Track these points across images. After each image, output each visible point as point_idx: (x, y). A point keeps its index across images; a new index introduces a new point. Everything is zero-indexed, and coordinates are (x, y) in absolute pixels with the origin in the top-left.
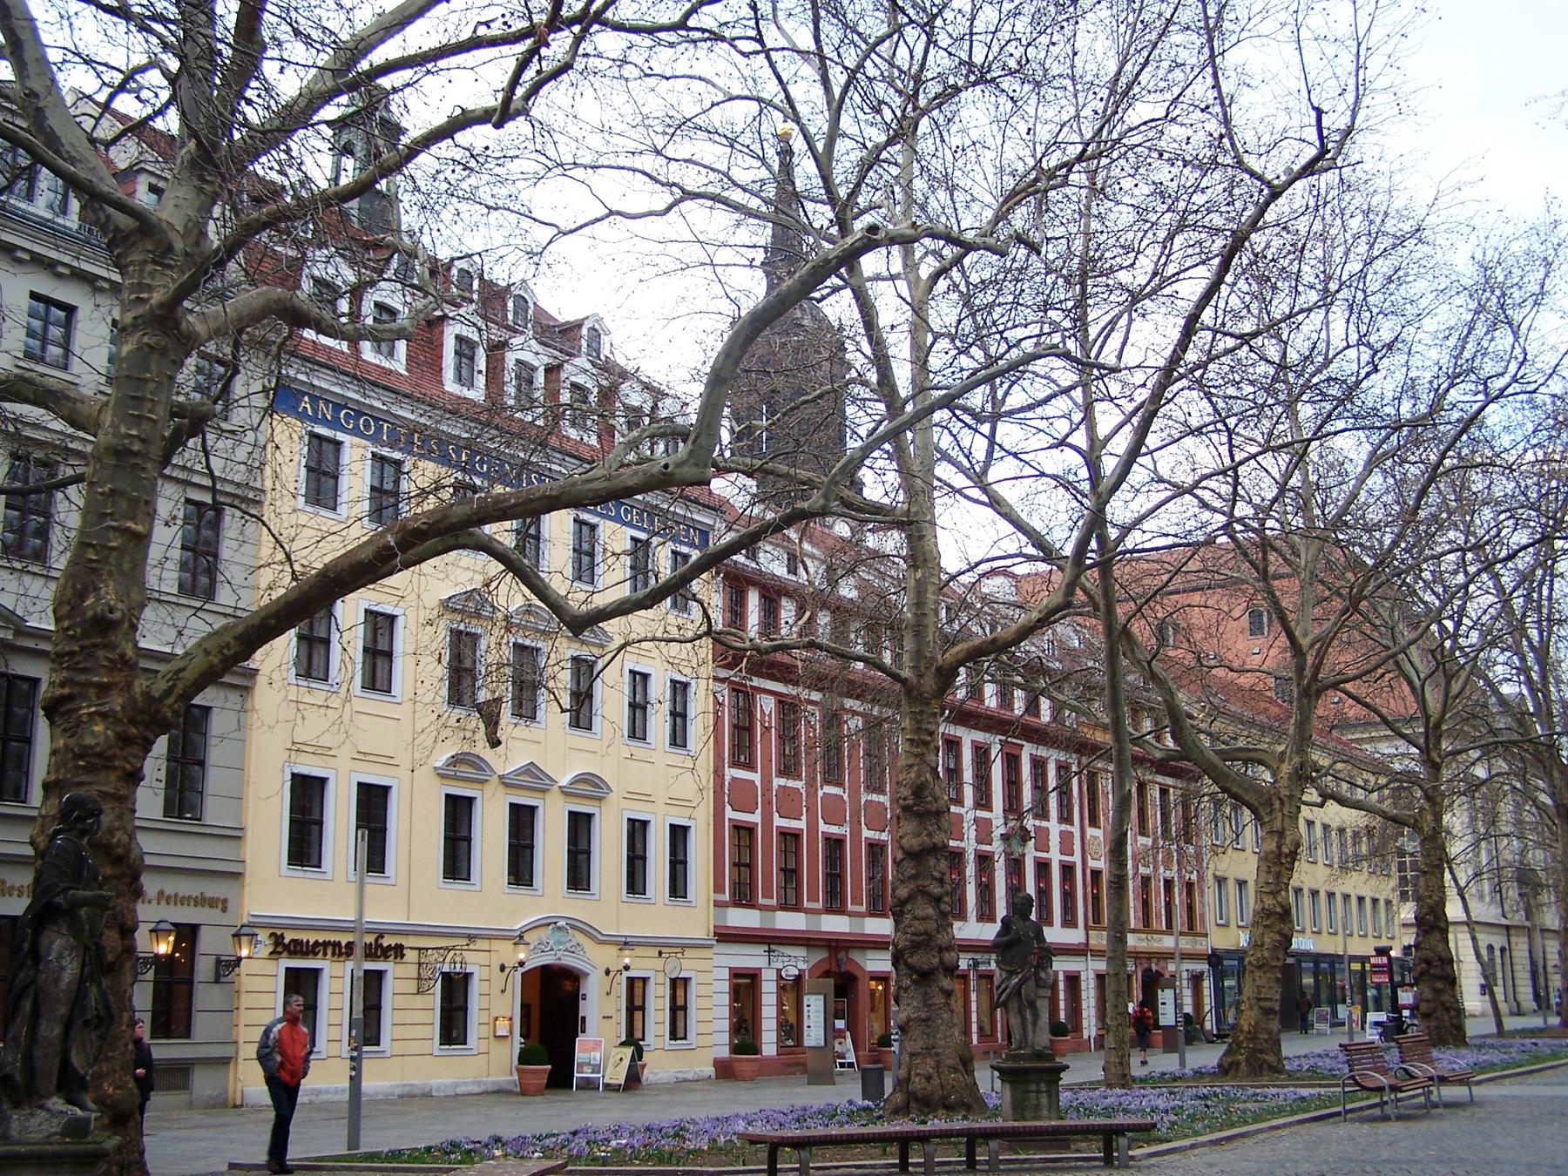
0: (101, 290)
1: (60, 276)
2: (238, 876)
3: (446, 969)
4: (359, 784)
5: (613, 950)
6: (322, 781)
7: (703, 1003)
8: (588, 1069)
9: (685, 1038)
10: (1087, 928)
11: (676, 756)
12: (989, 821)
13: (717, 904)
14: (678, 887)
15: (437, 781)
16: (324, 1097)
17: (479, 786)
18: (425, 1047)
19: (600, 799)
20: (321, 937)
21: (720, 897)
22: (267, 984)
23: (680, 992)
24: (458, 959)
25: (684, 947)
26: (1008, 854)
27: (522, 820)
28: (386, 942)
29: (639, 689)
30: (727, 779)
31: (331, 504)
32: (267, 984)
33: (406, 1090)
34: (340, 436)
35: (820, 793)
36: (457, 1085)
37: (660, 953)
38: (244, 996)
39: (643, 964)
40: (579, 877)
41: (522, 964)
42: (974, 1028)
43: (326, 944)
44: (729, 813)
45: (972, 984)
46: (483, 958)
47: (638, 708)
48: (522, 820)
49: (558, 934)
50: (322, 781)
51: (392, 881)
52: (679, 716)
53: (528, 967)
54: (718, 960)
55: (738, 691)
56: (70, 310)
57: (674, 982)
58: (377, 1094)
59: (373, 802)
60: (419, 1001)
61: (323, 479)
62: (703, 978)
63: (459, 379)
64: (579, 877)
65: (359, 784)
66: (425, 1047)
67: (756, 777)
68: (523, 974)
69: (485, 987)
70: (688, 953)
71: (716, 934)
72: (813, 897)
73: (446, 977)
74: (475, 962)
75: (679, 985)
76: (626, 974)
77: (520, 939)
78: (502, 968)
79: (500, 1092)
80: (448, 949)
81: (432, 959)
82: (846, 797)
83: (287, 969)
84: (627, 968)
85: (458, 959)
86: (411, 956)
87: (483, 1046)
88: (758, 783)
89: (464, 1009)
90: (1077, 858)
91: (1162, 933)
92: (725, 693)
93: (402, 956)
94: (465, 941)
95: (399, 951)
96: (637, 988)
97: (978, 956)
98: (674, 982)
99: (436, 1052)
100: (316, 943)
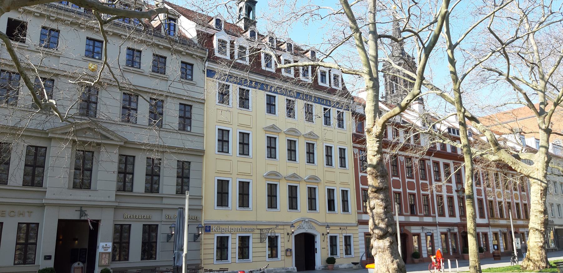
0: (82, 28)
1: (161, 48)
2: (201, 210)
3: (269, 235)
4: (239, 182)
7: (263, 250)
9: (351, 254)
10: (488, 218)
12: (451, 187)
13: (358, 213)
14: (345, 209)
15: (265, 180)
19: (318, 183)
23: (348, 240)
24: (273, 232)
25: (277, 225)
26: (458, 197)
27: (293, 191)
29: (329, 151)
31: (247, 107)
35: (391, 179)
37: (340, 228)
39: (333, 232)
40: (312, 206)
41: (293, 233)
42: (451, 250)
45: (449, 237)
46: (282, 231)
47: (329, 156)
48: (293, 191)
51: (300, 211)
52: (342, 158)
53: (296, 233)
54: (360, 230)
55: (435, 163)
56: (192, 65)
59: (244, 187)
60: (260, 245)
61: (271, 106)
62: (355, 236)
64: (312, 206)
65: (239, 182)
67: (414, 181)
68: (295, 236)
70: (348, 228)
72: (421, 212)
73: (269, 237)
74: (278, 232)
75: (347, 239)
77: (292, 226)
78: (288, 234)
80: (270, 229)
82: (400, 180)
83: (218, 237)
85: (273, 232)
88: (415, 182)
89: (336, 245)
90: (483, 197)
91: (499, 219)
94: (275, 226)
96: (333, 240)
97: (450, 228)
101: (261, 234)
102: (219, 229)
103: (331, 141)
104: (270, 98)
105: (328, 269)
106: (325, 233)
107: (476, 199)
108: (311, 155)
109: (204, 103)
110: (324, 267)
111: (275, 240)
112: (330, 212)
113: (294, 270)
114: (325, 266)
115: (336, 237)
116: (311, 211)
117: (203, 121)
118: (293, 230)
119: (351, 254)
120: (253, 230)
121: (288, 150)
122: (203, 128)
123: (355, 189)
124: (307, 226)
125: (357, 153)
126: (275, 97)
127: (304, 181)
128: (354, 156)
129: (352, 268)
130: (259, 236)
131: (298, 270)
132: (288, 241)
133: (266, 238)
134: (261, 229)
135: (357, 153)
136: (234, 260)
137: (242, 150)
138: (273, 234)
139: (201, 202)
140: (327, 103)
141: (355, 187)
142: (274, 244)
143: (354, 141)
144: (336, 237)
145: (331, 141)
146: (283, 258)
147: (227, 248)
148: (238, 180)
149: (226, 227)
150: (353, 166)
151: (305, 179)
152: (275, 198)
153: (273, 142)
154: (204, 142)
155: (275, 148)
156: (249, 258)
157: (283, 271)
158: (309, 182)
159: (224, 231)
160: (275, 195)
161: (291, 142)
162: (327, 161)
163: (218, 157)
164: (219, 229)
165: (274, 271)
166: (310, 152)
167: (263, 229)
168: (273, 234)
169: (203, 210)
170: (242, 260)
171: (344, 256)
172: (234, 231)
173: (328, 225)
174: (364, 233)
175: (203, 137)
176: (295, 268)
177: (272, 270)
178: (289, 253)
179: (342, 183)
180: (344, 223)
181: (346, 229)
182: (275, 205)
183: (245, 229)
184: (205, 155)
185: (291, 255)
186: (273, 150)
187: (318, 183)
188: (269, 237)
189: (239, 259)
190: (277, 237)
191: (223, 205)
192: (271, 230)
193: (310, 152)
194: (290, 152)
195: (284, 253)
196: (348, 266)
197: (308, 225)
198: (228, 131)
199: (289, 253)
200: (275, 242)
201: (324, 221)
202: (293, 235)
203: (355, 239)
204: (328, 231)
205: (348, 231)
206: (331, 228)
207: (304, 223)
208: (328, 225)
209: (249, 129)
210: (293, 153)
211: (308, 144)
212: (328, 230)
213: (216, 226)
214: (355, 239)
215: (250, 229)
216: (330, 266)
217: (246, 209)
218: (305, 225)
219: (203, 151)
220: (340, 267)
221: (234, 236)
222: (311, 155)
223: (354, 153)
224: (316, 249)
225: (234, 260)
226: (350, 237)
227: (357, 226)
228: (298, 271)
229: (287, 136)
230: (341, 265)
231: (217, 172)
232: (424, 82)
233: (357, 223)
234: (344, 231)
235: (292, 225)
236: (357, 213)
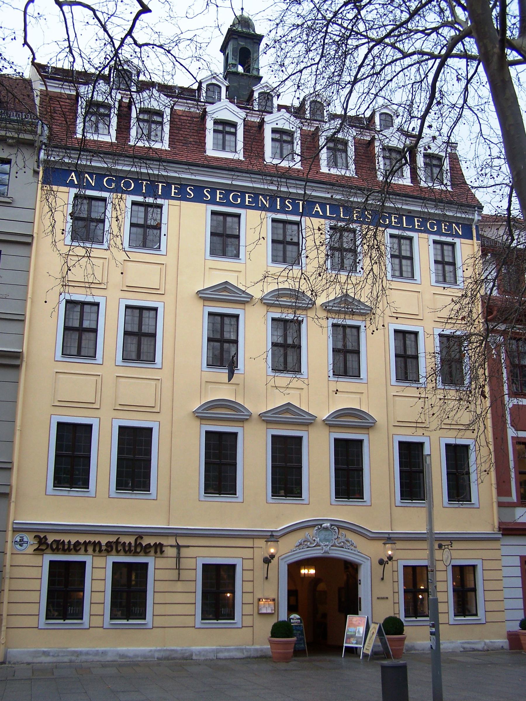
5: (380, 544)
6: (150, 430)
8: (353, 641)
9: (476, 615)
13: (501, 505)
15: (198, 422)
16: (83, 658)
17: (365, 431)
18: (189, 621)
20: (82, 539)
22: (34, 573)
28: (145, 542)
32: (34, 573)
33: (167, 654)
34: (159, 201)
36: (218, 651)
38: (7, 581)
43: (86, 544)
44: (511, 432)
46: (247, 553)
49: (324, 534)
50: (150, 430)
54: (505, 550)
58: (137, 656)
62: (488, 565)
66: (189, 621)
69: (248, 576)
70: (455, 545)
71: (500, 529)
79: (262, 658)
86: (171, 552)
87: (248, 621)
93: (162, 552)
95: (159, 548)
100: (78, 543)
104: (225, 221)
107: (421, 441)
109: (30, 244)
119: (476, 615)
126: (238, 216)
136: (97, 621)
139: (10, 477)
148: (117, 424)
161: (285, 330)
163: (122, 372)
174: (521, 557)
175: (23, 321)
198: (416, 334)
203: (488, 575)
214: (488, 575)
219: (18, 356)
224: (360, 598)
225: (97, 621)
229: (207, 303)
232: (68, 50)
236: (495, 505)
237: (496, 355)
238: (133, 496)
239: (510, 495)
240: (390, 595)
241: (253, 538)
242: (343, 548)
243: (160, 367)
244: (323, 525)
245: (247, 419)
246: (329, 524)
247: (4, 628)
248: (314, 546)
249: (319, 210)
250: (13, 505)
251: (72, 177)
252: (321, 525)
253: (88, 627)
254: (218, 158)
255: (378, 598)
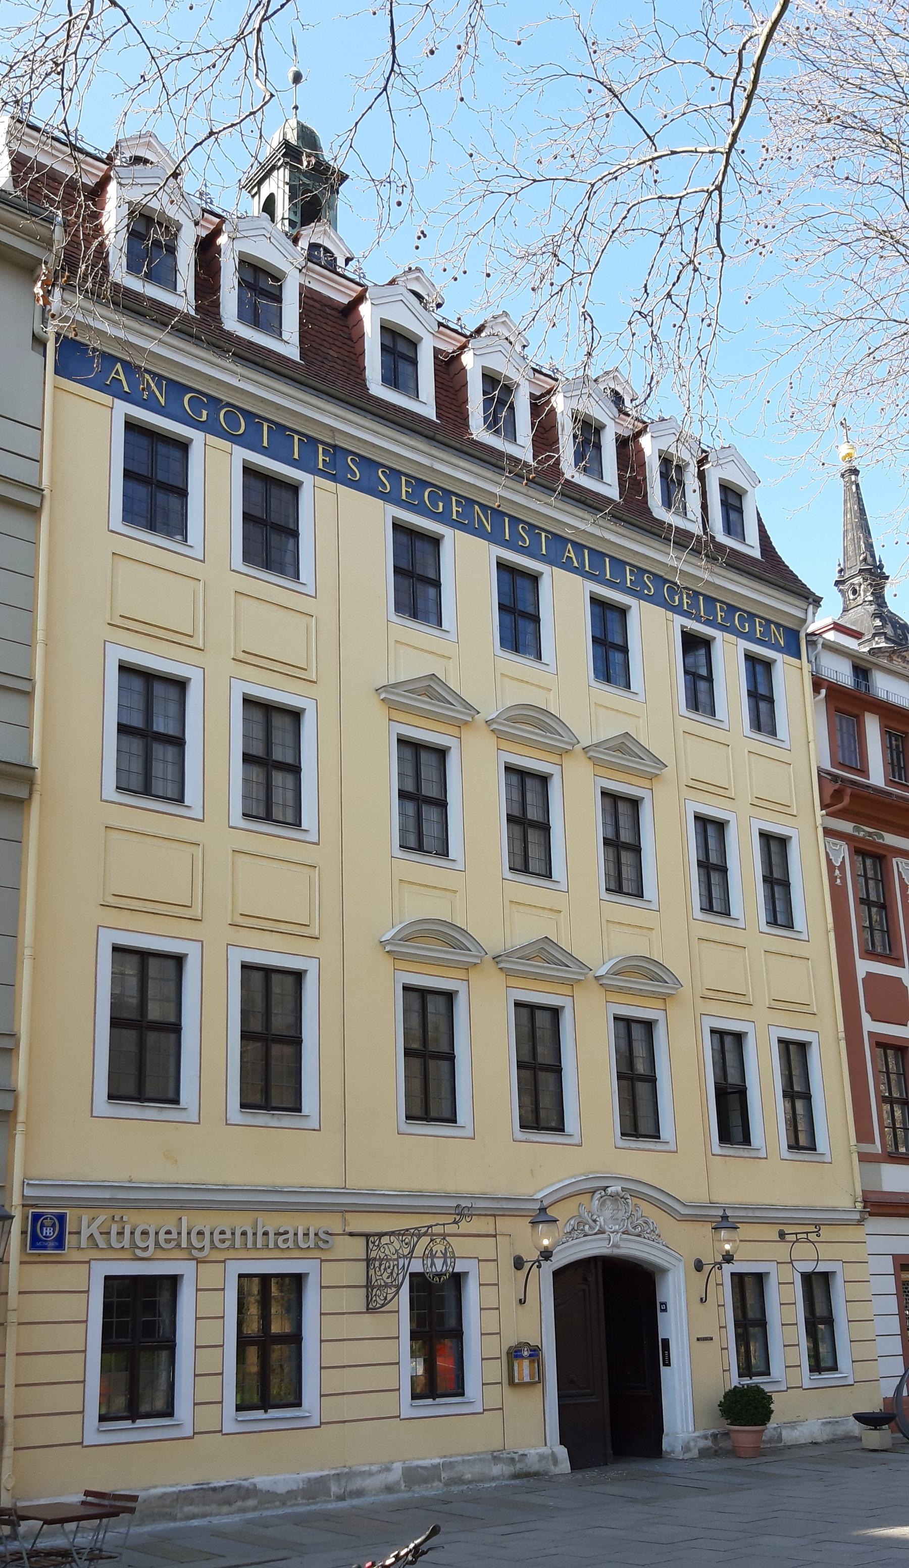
3: (417, 1266)
9: (834, 1368)
11: (777, 939)
13: (864, 1158)
15: (386, 964)
19: (664, 998)
21: (867, 1148)
23: (818, 1293)
24: (439, 1248)
25: (461, 1213)
30: (861, 975)
37: (782, 1235)
38: (12, 1332)
41: (547, 1254)
44: (869, 1025)
46: (485, 1248)
51: (576, 1140)
53: (560, 1260)
54: (876, 1244)
57: (807, 1278)
60: (368, 1324)
62: (853, 1272)
63: (492, 424)
68: (557, 1274)
70: (826, 1233)
73: (419, 1282)
76: (728, 1269)
78: (519, 1263)
81: (389, 1251)
83: (107, 1278)
84: (728, 1258)
85: (439, 1248)
89: (762, 1323)
92: (841, 853)
98: (807, 1278)
99: (406, 1412)
101: (369, 1261)
102: (120, 1233)
103: (721, 792)
105: (733, 1453)
106: (707, 1259)
108: (627, 857)
109: (34, 512)
110: (709, 1443)
111: (450, 1294)
112: (729, 1150)
113: (555, 1462)
114: (714, 1436)
115: (760, 1278)
116: (632, 1143)
117: (31, 611)
118: (546, 1242)
119: (834, 1368)
120: (323, 1240)
121: (511, 819)
122: (30, 646)
123: (842, 1035)
124: (614, 1219)
125: (843, 862)
127: (594, 983)
128: (832, 879)
129: (859, 1439)
130: (357, 1273)
131: (576, 1463)
132: (522, 1302)
133: (399, 1287)
134: (367, 1236)
135: (843, 862)
136: (208, 1418)
137: (262, 796)
138: (439, 1263)
140: (694, 604)
141: (841, 1027)
142: (441, 1317)
143: (828, 800)
144: (760, 1278)
145: (721, 792)
146: (494, 1396)
147: (170, 1346)
148: (237, 957)
149: (167, 1220)
150: (831, 925)
151: (602, 971)
152: (444, 1065)
153: (428, 772)
154: (28, 727)
155: (442, 804)
156: (299, 1405)
157: (497, 1470)
158: (620, 990)
159: (151, 1242)
160: (444, 1048)
162: (704, 892)
164: (120, 1233)
165: (444, 1475)
166: (623, 839)
167: (381, 1235)
168: (439, 1263)
169: (21, 1117)
170: (259, 1414)
171: (806, 1377)
172: (213, 1247)
173: (725, 1218)
174: (895, 1256)
175: (28, 694)
176: (562, 1452)
177: (436, 1467)
178: (524, 1369)
179: (779, 1005)
180: (797, 1209)
181: (812, 1237)
182: (446, 1103)
183: (278, 1234)
184: (36, 798)
185: (539, 1379)
186: (430, 814)
187: (664, 998)
188: (419, 1282)
189: (239, 1408)
190: (458, 1279)
191: (149, 1094)
192: (425, 1240)
193: (623, 839)
194: (518, 830)
195: (497, 1371)
196: (828, 1428)
197: (621, 1215)
199: (524, 1369)
200: (451, 1308)
201: (704, 1198)
202: (549, 1268)
204: (727, 1247)
205: (825, 1251)
206: (745, 1231)
207: (603, 1204)
208: (725, 1218)
209: (299, 686)
210: (533, 836)
211: (624, 1023)
212: (728, 1241)
213: (103, 1216)
215: (306, 1235)
216: (744, 1434)
217: (287, 1120)
218: (608, 1213)
220: (790, 1436)
221: (210, 1275)
222: (627, 857)
223: (829, 861)
224: (666, 1342)
226: (826, 1277)
227: (860, 1222)
228: (574, 1466)
230: (793, 1425)
231: (114, 901)
233: (860, 1206)
234: (803, 1250)
235: (543, 1210)
236: (855, 1157)
237: (840, 878)
238: (274, 1122)
239: (873, 1142)
240: (713, 1332)
241: (494, 1216)
242: (639, 1236)
243: (315, 840)
244: (609, 1190)
245: (475, 964)
246: (619, 1188)
247: (8, 1451)
248: (596, 1234)
249: (572, 555)
250: (19, 1140)
251: (117, 373)
252: (605, 1189)
253: (319, 1424)
254: (400, 408)
255: (698, 1339)
